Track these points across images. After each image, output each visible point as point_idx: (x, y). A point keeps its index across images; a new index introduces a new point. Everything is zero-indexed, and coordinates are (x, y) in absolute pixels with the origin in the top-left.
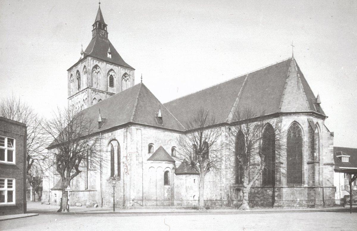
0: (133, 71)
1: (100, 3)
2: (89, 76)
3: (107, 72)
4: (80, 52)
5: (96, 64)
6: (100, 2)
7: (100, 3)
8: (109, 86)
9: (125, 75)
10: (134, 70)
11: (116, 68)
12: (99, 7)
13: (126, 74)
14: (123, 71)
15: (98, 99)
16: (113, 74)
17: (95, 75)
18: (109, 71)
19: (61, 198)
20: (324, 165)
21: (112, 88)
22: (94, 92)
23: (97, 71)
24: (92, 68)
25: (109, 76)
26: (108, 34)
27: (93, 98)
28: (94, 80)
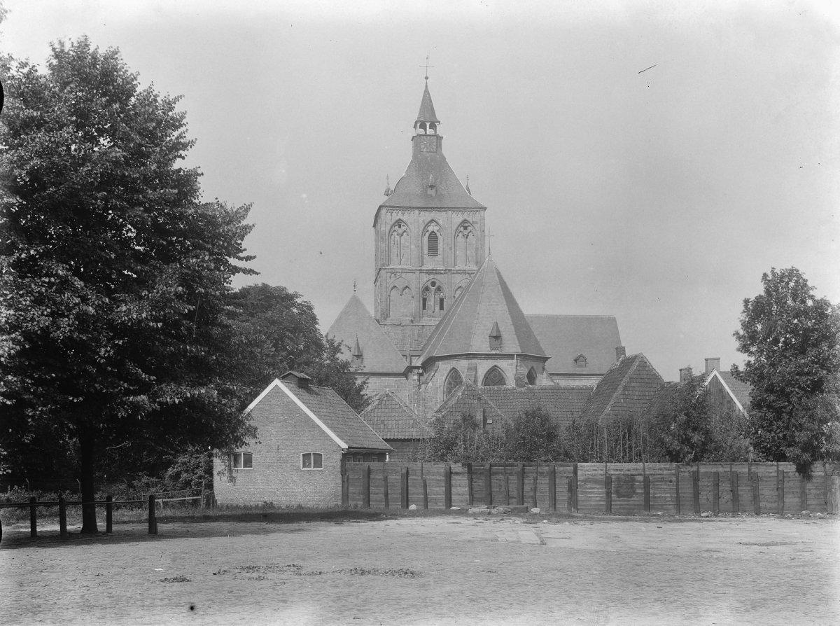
0: (482, 212)
1: (427, 78)
2: (383, 245)
3: (421, 229)
4: (383, 190)
5: (398, 218)
6: (428, 76)
7: (427, 78)
8: (426, 256)
9: (464, 224)
10: (485, 209)
11: (441, 217)
12: (426, 86)
13: (465, 221)
14: (458, 218)
15: (401, 287)
16: (436, 229)
17: (396, 239)
18: (427, 225)
19: (246, 261)
20: (424, 307)
21: (434, 258)
22: (393, 275)
23: (400, 231)
24: (388, 227)
25: (427, 234)
26: (443, 141)
27: (391, 286)
28: (394, 250)
